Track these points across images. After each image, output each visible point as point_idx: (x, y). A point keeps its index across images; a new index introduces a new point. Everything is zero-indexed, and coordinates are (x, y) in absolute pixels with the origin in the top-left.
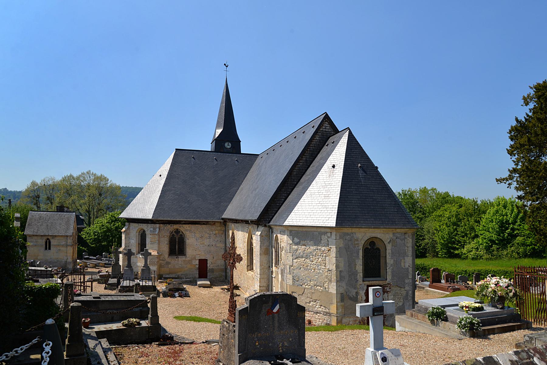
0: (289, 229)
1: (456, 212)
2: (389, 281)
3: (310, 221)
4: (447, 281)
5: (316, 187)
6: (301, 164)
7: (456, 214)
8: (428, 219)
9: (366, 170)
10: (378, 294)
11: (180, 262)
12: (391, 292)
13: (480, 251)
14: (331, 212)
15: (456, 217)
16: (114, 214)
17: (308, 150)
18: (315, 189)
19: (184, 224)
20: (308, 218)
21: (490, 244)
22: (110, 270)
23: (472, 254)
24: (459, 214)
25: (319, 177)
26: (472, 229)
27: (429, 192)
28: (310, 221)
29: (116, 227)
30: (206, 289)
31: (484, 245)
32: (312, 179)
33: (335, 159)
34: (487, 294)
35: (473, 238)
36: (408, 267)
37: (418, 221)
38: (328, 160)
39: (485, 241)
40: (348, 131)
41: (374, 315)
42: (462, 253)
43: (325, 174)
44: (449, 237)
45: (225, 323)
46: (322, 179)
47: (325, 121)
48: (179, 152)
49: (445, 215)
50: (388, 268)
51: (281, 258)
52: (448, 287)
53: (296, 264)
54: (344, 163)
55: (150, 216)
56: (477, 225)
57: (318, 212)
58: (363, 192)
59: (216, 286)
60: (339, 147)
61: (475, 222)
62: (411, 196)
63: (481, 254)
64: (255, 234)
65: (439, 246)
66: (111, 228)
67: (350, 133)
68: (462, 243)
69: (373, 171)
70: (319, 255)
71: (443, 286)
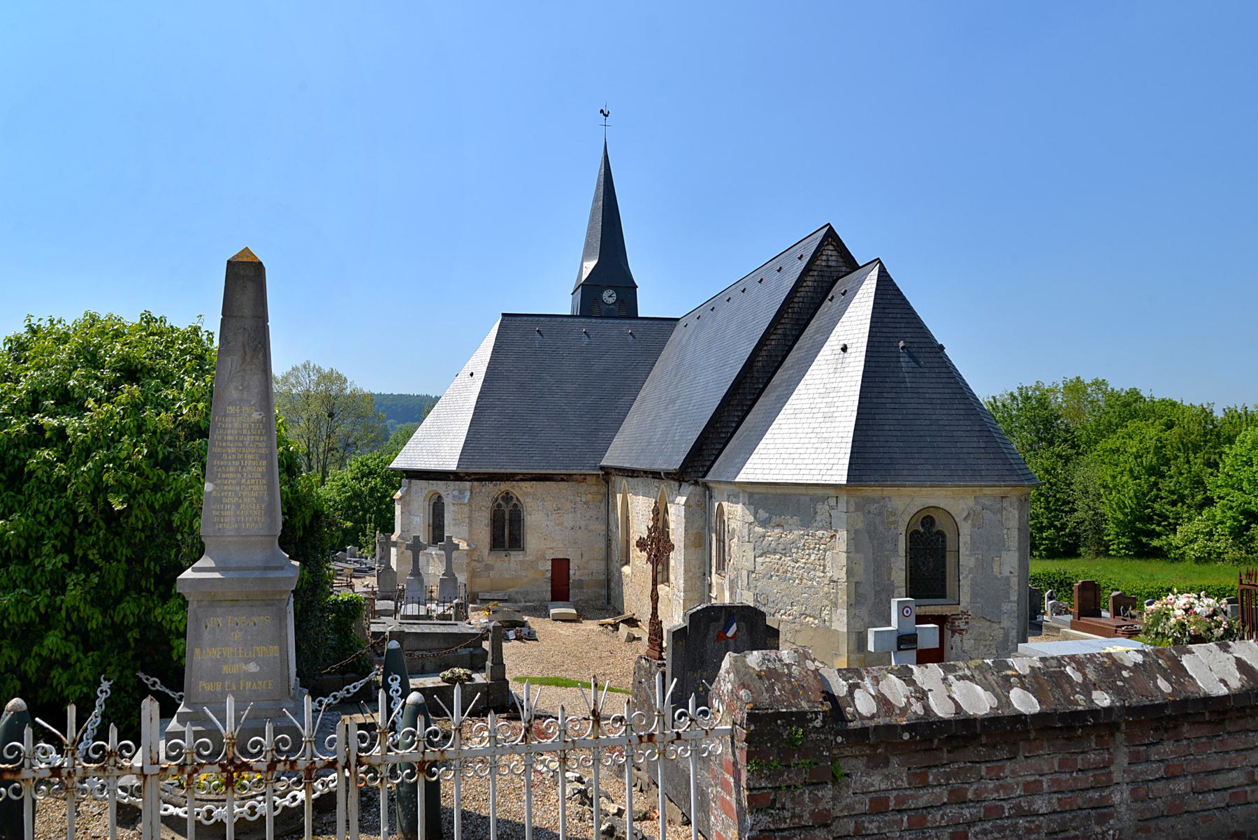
0: (748, 490)
1: (1156, 440)
2: (964, 607)
3: (792, 472)
4: (1116, 613)
5: (806, 396)
6: (773, 343)
7: (1156, 447)
8: (1085, 458)
9: (915, 355)
10: (907, 612)
11: (513, 565)
12: (970, 631)
13: (1218, 541)
14: (837, 450)
15: (1155, 454)
16: (367, 460)
17: (790, 311)
18: (803, 401)
19: (522, 480)
20: (789, 467)
21: (1244, 523)
22: (372, 581)
23: (1196, 547)
24: (1165, 447)
25: (814, 372)
26: (1198, 483)
27: (1089, 391)
28: (792, 472)
29: (372, 488)
30: (569, 624)
31: (1228, 525)
32: (797, 379)
33: (847, 333)
34: (1166, 632)
35: (1200, 507)
36: (1008, 574)
37: (1060, 464)
38: (833, 334)
39: (1229, 513)
40: (878, 266)
41: (899, 649)
42: (1171, 544)
43: (826, 367)
44: (1138, 504)
45: (643, 661)
46: (819, 377)
47: (828, 244)
48: (509, 319)
49: (1128, 449)
50: (963, 578)
51: (730, 555)
52: (1118, 627)
53: (762, 568)
54: (866, 339)
55: (452, 465)
56: (1211, 474)
57: (809, 451)
58: (908, 406)
59: (588, 619)
60: (857, 305)
61: (1204, 464)
62: (1042, 403)
63: (1219, 548)
64: (673, 502)
65: (1111, 528)
66: (361, 490)
67: (883, 272)
68: (1171, 521)
69: (932, 355)
70: (811, 546)
71: (1104, 624)
